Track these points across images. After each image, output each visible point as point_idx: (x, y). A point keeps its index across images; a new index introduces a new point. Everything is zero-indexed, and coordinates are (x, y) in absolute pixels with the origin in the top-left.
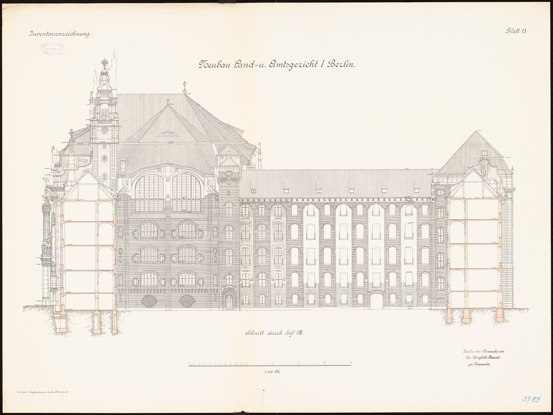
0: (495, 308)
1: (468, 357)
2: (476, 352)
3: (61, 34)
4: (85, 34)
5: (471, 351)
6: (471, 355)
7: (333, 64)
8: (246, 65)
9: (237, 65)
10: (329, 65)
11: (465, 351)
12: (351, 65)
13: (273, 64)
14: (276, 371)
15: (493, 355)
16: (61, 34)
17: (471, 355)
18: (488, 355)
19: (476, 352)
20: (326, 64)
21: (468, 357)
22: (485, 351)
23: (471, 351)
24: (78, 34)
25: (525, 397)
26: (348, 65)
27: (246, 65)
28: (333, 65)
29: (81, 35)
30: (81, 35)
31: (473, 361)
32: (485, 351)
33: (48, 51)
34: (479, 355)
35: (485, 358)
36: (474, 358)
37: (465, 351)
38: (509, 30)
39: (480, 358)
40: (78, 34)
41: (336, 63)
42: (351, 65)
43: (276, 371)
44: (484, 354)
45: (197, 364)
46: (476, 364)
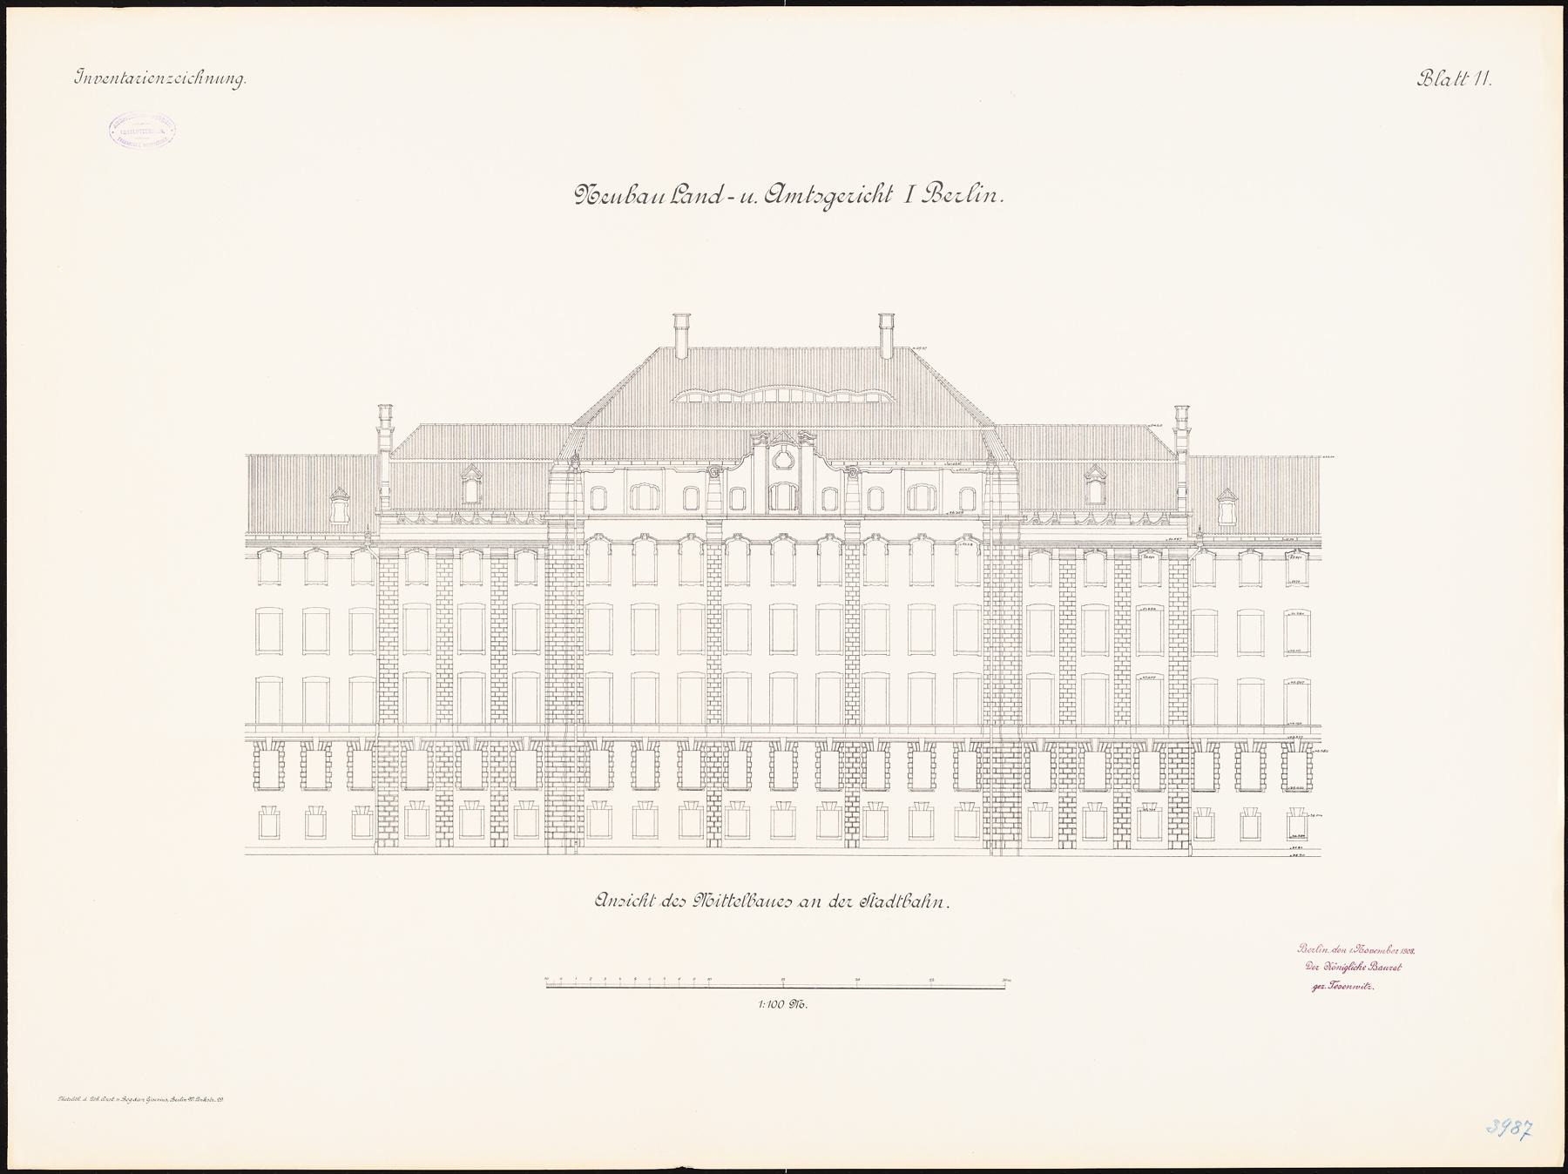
0: (983, 434)
1: (1311, 967)
2: (1336, 950)
3: (160, 79)
4: (231, 79)
5: (1321, 949)
6: (1320, 959)
7: (937, 191)
8: (703, 198)
9: (678, 197)
10: (928, 196)
11: (1304, 948)
12: (991, 197)
13: (778, 194)
14: (795, 1003)
15: (1383, 960)
16: (160, 79)
17: (1320, 959)
18: (1368, 959)
19: (1336, 950)
20: (920, 193)
21: (1311, 967)
22: (1360, 949)
23: (1321, 949)
24: (210, 79)
25: (1497, 1122)
26: (977, 194)
27: (703, 198)
28: (937, 197)
29: (220, 80)
30: (220, 80)
31: (1325, 977)
32: (1360, 949)
33: (126, 138)
34: (1343, 960)
35: (1359, 967)
36: (1329, 967)
37: (1304, 948)
38: (1427, 75)
39: (1345, 969)
40: (210, 79)
41: (944, 192)
42: (991, 197)
43: (795, 1003)
44: (1358, 958)
45: (584, 981)
46: (1335, 985)
